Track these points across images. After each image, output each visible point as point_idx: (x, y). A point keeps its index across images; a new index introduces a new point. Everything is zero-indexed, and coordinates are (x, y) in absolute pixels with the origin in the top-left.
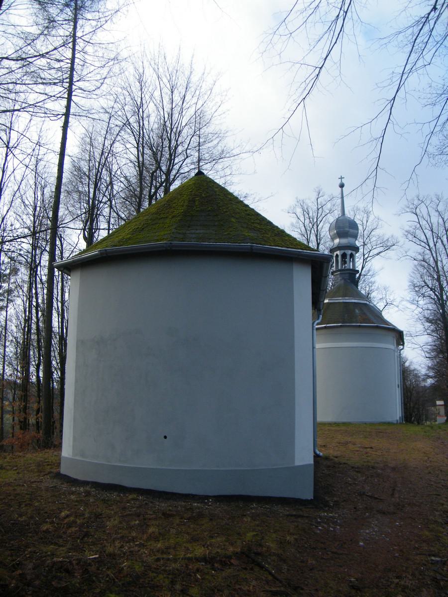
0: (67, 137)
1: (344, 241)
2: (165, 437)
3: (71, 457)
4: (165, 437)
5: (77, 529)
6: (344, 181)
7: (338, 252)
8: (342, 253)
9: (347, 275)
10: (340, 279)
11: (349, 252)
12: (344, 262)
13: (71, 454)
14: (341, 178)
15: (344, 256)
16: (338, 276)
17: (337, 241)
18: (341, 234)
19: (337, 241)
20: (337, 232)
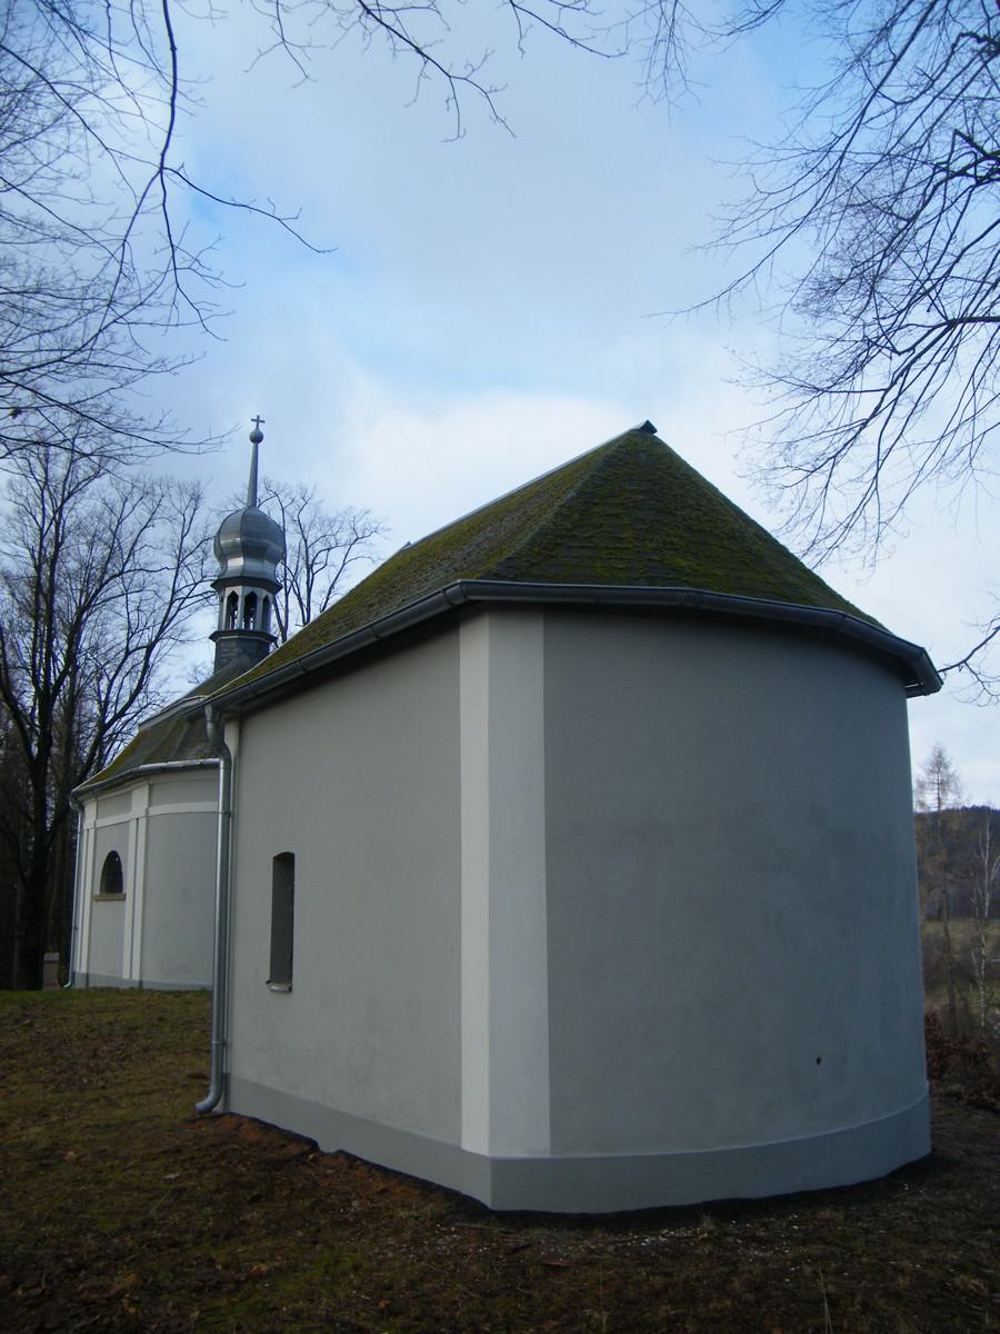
0: (847, 599)
1: (255, 566)
2: (819, 1061)
3: (548, 1156)
4: (819, 1061)
5: (550, 1279)
6: (262, 428)
7: (239, 590)
8: (246, 594)
9: (255, 645)
10: (236, 650)
11: (262, 593)
12: (248, 614)
13: (547, 1145)
14: (258, 421)
15: (251, 600)
16: (234, 644)
17: (237, 563)
18: (250, 549)
19: (237, 563)
20: (242, 542)
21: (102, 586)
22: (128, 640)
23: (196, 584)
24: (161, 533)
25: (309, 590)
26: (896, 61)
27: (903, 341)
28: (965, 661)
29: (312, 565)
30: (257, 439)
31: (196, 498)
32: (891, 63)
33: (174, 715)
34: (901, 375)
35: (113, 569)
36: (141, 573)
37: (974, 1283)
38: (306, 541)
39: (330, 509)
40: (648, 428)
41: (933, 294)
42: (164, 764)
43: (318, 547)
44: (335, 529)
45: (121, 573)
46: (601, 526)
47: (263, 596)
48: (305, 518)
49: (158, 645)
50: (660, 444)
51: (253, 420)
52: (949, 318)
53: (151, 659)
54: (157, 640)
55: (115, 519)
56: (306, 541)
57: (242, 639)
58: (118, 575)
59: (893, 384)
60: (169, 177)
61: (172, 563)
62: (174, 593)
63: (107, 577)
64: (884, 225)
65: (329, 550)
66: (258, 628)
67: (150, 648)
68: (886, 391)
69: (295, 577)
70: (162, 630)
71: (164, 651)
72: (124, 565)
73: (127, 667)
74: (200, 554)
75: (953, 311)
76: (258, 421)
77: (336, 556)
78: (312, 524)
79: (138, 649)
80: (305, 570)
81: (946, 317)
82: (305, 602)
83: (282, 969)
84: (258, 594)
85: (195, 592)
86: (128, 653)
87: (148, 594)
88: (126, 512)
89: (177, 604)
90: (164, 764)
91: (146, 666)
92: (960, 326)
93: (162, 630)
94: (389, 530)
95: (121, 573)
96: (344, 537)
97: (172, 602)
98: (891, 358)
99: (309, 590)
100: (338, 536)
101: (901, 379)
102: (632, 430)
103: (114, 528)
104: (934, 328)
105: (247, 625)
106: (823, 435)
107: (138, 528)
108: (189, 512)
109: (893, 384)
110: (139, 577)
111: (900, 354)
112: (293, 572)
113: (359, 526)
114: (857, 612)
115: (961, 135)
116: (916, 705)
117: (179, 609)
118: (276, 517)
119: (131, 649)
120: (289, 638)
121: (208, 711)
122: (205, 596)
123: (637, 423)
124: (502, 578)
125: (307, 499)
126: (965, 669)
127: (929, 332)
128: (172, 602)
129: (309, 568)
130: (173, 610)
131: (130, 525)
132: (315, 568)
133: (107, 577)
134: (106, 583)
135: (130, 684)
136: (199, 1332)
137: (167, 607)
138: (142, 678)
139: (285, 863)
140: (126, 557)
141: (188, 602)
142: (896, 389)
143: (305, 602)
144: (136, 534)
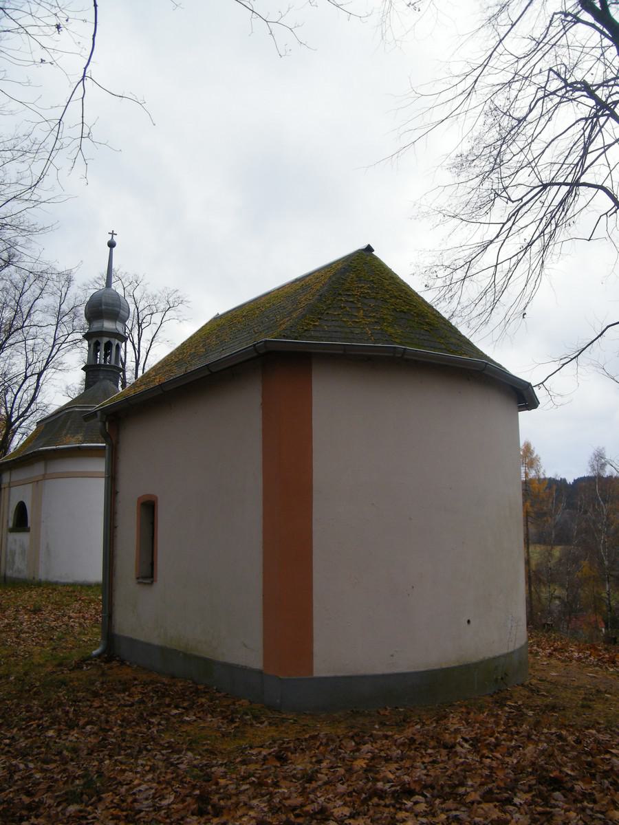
21: (10, 335)
22: (26, 369)
23: (69, 335)
24: (48, 301)
25: (139, 339)
26: (513, 25)
27: (516, 194)
28: (542, 383)
29: (141, 324)
30: (112, 245)
31: (69, 280)
32: (510, 26)
33: (61, 416)
34: (513, 215)
35: (17, 324)
36: (34, 327)
37: (585, 722)
38: (138, 309)
39: (152, 289)
40: (369, 249)
41: (533, 164)
42: (55, 447)
43: (146, 312)
44: (156, 301)
45: (22, 327)
46: (345, 307)
47: (116, 343)
48: (137, 294)
49: (45, 372)
50: (376, 258)
51: (116, 234)
52: (544, 183)
53: (41, 381)
54: (44, 369)
55: (18, 293)
56: (138, 309)
57: (100, 371)
58: (20, 329)
59: (508, 220)
60: (88, 82)
61: (54, 321)
62: (55, 340)
63: (13, 330)
64: (506, 122)
65: (152, 314)
66: (113, 363)
67: (40, 374)
68: (504, 224)
69: (131, 331)
70: (47, 363)
71: (48, 377)
72: (24, 322)
73: (25, 387)
74: (72, 315)
75: (546, 177)
76: (113, 234)
77: (157, 318)
78: (142, 298)
79: (32, 375)
80: (137, 327)
81: (542, 182)
82: (137, 346)
83: (148, 574)
84: (113, 342)
85: (68, 340)
86: (26, 377)
87: (39, 341)
88: (26, 288)
89: (57, 346)
90: (55, 447)
91: (38, 386)
92: (549, 187)
93: (47, 363)
94: (189, 302)
95: (22, 327)
96: (162, 306)
97: (53, 346)
98: (507, 203)
99: (139, 339)
100: (158, 305)
101: (514, 217)
102: (359, 250)
103: (17, 298)
104: (535, 188)
105: (105, 362)
106: (463, 248)
107: (32, 299)
108: (64, 290)
109: (508, 220)
110: (33, 330)
111: (513, 202)
112: (130, 328)
113: (171, 300)
114: (492, 361)
115: (553, 71)
116: (524, 416)
117: (58, 350)
118: (120, 291)
119: (28, 375)
120: (145, 372)
121: (99, 413)
122: (75, 342)
123: (363, 245)
124: (287, 338)
125: (138, 282)
126: (543, 388)
127: (531, 190)
128: (53, 346)
129: (140, 326)
130: (55, 350)
131: (28, 296)
132: (143, 326)
133: (13, 330)
134: (13, 333)
135: (27, 397)
136: (8, 824)
137: (51, 348)
138: (35, 394)
139: (149, 507)
140: (25, 317)
141: (64, 346)
142: (510, 223)
143: (137, 346)
144: (32, 302)
